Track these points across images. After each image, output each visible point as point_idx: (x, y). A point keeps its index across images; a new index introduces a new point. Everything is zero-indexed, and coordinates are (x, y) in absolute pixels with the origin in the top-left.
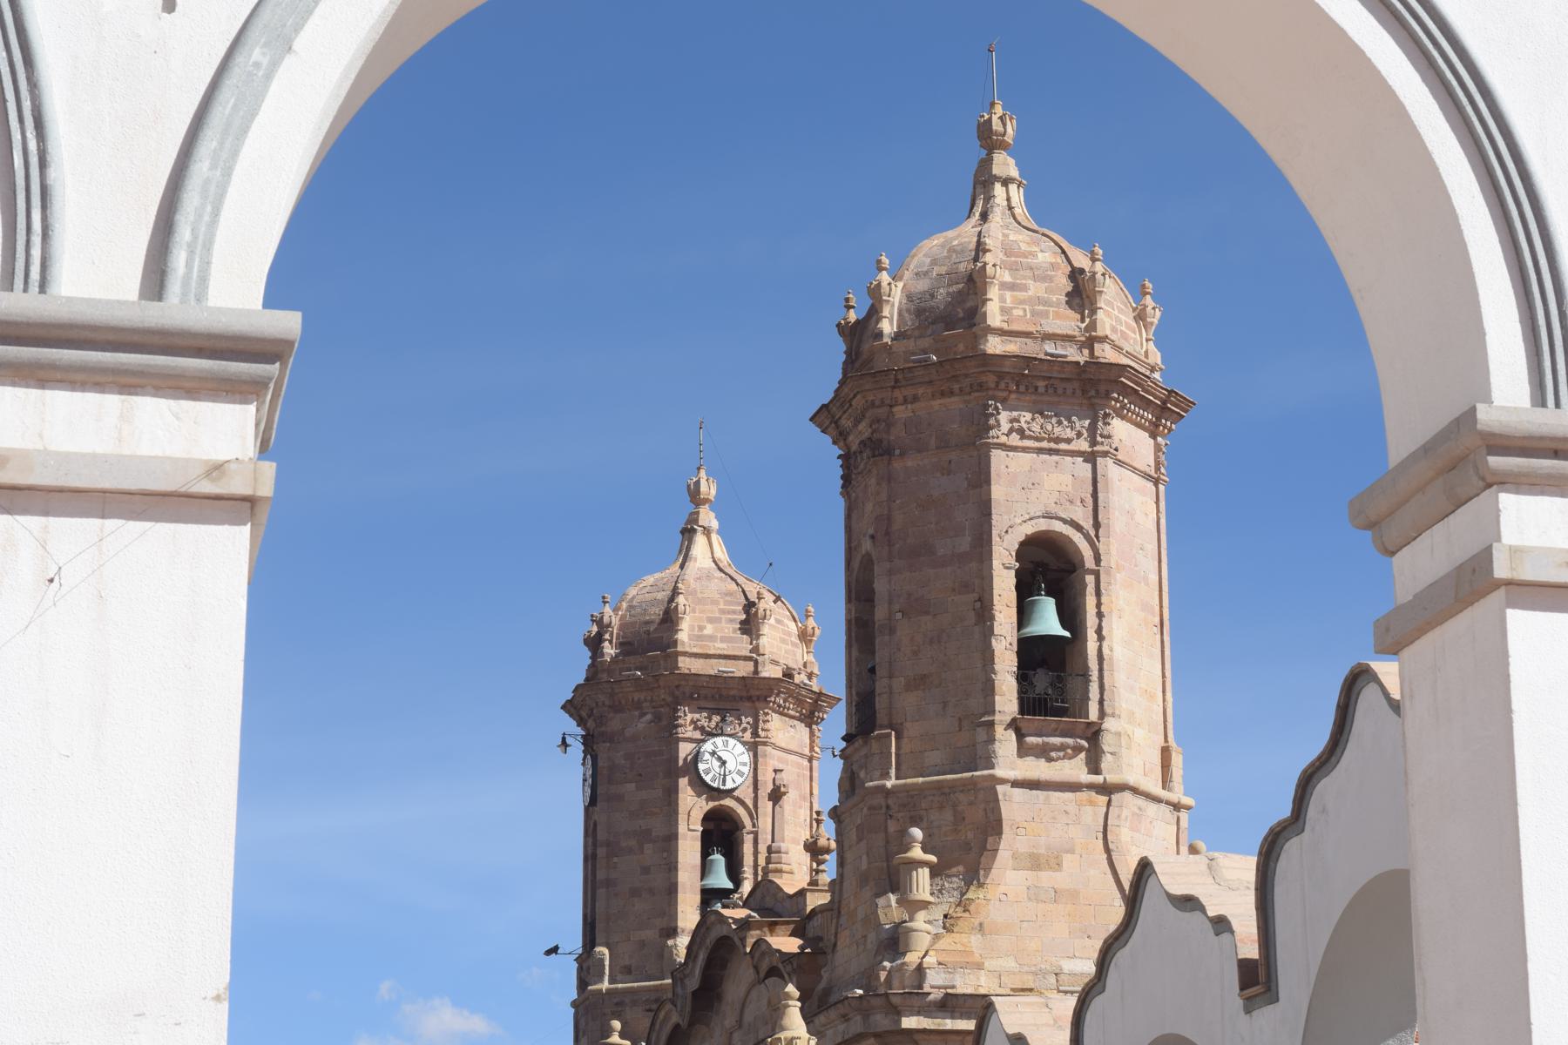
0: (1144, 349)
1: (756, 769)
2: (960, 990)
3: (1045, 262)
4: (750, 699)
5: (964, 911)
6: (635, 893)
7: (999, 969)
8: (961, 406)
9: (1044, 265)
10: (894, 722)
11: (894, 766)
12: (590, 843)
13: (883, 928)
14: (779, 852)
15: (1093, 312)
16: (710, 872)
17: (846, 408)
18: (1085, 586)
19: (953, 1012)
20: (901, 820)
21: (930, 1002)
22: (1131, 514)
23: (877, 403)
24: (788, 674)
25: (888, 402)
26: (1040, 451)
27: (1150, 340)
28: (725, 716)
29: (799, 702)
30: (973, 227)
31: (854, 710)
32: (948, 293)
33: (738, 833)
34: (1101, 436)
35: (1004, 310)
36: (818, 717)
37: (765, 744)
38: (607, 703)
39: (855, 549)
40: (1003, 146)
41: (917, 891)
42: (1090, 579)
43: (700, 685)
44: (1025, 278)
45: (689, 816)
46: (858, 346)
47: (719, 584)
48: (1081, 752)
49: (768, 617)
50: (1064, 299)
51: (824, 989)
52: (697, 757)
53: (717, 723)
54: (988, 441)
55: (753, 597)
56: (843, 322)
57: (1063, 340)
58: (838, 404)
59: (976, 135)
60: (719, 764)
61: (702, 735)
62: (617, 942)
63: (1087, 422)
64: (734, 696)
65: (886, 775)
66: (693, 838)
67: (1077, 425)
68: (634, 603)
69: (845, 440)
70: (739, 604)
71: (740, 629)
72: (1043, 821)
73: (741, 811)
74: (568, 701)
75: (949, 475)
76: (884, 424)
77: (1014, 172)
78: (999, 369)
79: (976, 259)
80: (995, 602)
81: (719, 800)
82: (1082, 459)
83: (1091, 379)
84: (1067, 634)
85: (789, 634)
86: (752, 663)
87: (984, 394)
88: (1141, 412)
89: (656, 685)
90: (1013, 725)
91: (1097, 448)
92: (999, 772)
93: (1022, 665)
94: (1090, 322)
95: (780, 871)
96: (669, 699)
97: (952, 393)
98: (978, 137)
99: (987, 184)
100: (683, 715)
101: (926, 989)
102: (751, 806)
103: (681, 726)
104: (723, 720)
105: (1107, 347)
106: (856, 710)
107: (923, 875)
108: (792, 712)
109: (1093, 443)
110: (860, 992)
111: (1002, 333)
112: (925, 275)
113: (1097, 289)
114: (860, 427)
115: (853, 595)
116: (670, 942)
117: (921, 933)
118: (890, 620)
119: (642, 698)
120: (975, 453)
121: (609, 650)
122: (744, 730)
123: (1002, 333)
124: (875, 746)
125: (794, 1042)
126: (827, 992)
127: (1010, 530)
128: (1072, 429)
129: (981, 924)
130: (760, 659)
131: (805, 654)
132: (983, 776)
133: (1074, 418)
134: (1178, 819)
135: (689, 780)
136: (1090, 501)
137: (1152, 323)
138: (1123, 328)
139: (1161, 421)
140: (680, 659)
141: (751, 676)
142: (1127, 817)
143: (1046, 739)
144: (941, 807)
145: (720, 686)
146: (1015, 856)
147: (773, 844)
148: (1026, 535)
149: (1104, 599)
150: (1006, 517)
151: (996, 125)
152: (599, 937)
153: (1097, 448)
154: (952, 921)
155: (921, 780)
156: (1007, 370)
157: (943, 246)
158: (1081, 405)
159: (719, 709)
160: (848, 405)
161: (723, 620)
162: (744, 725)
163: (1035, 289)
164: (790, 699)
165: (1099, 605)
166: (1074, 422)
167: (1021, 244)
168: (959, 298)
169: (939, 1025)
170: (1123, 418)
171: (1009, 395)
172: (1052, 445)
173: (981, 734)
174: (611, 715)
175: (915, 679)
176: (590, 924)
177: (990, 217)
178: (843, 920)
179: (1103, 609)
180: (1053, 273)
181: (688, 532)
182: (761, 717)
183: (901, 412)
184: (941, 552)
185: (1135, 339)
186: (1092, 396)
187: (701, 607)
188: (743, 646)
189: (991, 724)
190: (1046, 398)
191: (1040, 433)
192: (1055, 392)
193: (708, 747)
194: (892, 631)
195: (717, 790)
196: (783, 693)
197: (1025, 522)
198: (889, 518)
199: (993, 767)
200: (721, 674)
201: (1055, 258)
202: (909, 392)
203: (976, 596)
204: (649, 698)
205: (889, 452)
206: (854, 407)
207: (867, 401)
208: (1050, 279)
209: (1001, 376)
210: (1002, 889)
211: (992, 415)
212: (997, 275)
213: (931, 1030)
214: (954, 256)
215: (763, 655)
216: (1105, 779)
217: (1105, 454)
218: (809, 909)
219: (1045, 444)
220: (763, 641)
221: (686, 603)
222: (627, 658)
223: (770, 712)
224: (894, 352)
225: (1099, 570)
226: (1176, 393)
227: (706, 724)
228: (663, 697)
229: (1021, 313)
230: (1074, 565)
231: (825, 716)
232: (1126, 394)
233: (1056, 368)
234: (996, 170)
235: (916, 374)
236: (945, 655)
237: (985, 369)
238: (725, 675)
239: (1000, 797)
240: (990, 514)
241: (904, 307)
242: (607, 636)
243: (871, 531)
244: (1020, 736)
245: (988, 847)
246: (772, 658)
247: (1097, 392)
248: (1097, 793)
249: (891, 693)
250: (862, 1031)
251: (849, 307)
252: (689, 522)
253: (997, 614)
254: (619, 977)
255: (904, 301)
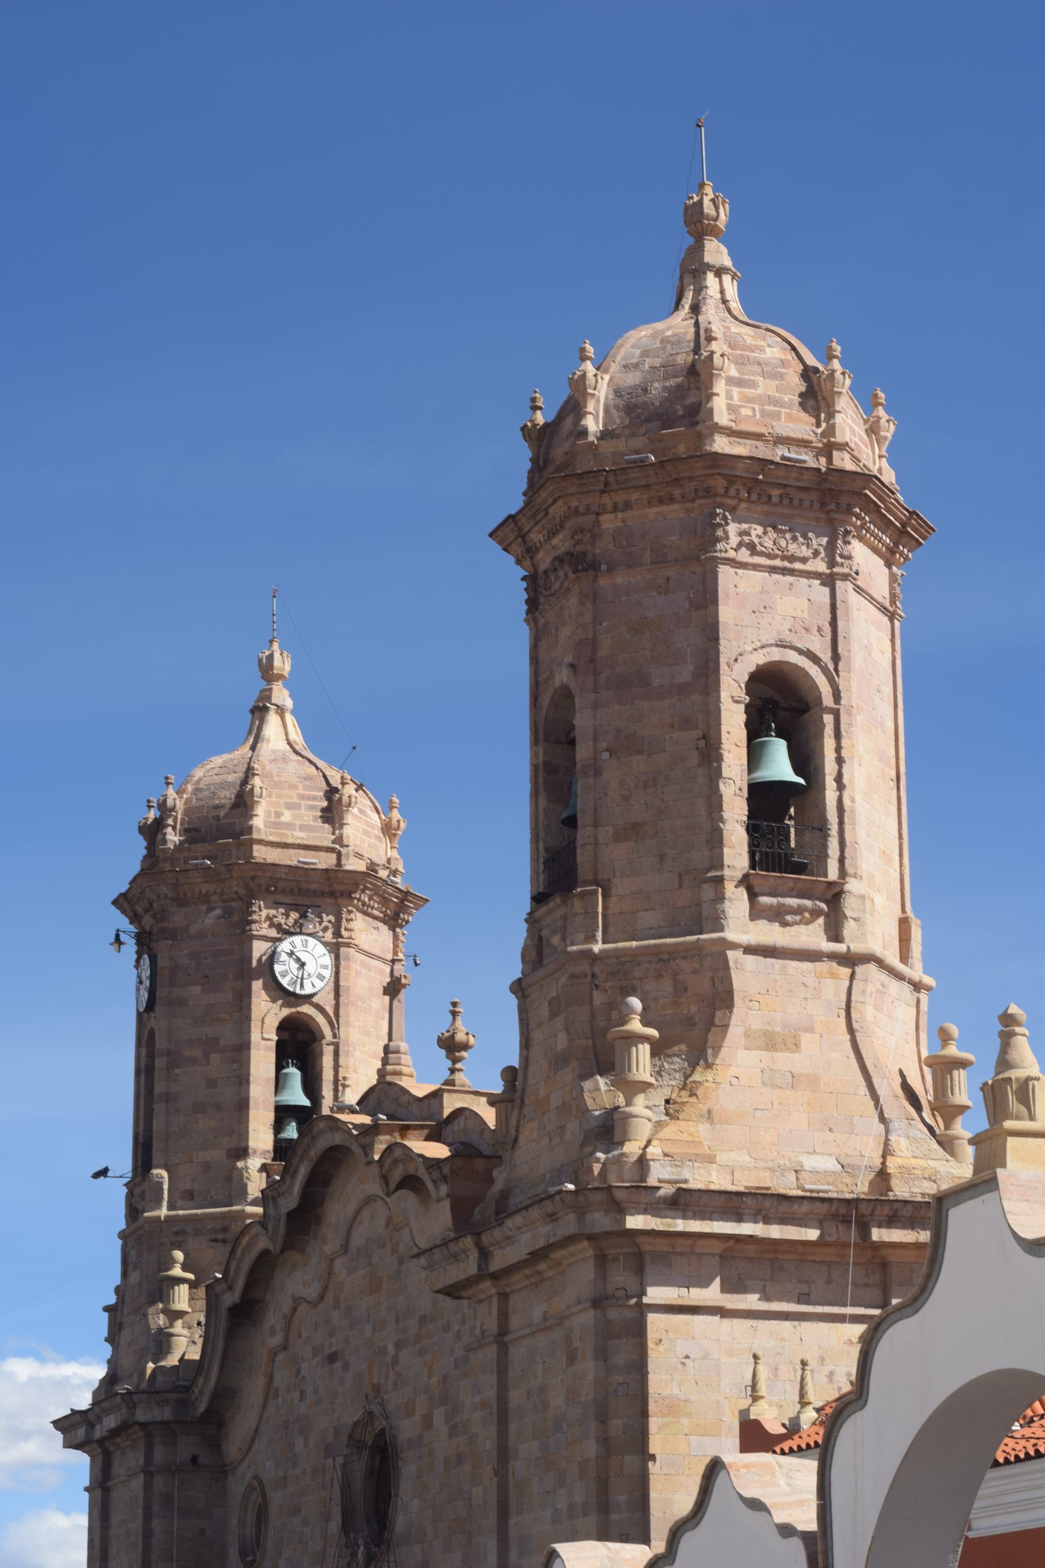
0: (877, 467)
1: (337, 974)
2: (693, 1185)
3: (775, 359)
4: (332, 894)
5: (691, 1095)
6: (199, 1108)
7: (731, 1164)
8: (682, 515)
9: (773, 361)
10: (600, 878)
11: (600, 929)
12: (144, 1054)
13: (592, 1115)
14: (398, 1052)
15: (831, 415)
16: (283, 1088)
17: (539, 518)
18: (822, 726)
19: (684, 1211)
20: (609, 991)
21: (660, 1198)
22: (868, 649)
23: (582, 510)
24: (372, 867)
25: (595, 508)
26: (773, 570)
27: (883, 456)
28: (306, 912)
29: (385, 901)
30: (683, 320)
31: (541, 867)
32: (664, 388)
33: (315, 1045)
34: (841, 556)
35: (731, 408)
36: (403, 920)
37: (348, 945)
38: (170, 895)
39: (546, 682)
40: (714, 232)
41: (637, 1071)
42: (828, 719)
43: (278, 876)
44: (753, 373)
45: (263, 1022)
46: (547, 453)
47: (296, 768)
48: (819, 916)
49: (353, 804)
50: (797, 399)
51: (501, 1192)
52: (272, 958)
53: (296, 922)
54: (715, 554)
55: (336, 782)
56: (529, 424)
57: (797, 446)
58: (530, 514)
59: (682, 219)
60: (298, 966)
61: (278, 933)
62: (178, 1164)
63: (824, 540)
64: (315, 891)
65: (592, 938)
66: (267, 1049)
67: (814, 542)
68: (201, 785)
69: (532, 558)
70: (319, 789)
71: (321, 817)
72: (779, 994)
73: (320, 1019)
74: (122, 895)
75: (666, 594)
76: (589, 534)
77: (728, 262)
78: (731, 472)
79: (696, 350)
80: (724, 740)
81: (296, 1007)
82: (819, 582)
83: (833, 490)
84: (801, 781)
85: (372, 826)
86: (334, 855)
87: (711, 501)
88: (880, 534)
89: (228, 876)
90: (745, 882)
91: (836, 570)
92: (731, 934)
93: (753, 813)
94: (826, 427)
95: (399, 1074)
96: (242, 892)
97: (671, 500)
98: (685, 222)
99: (697, 274)
100: (257, 910)
101: (652, 1181)
102: (332, 1015)
103: (255, 922)
104: (304, 916)
105: (847, 456)
106: (545, 868)
107: (644, 1051)
108: (376, 913)
109: (832, 563)
110: (571, 1187)
111: (731, 433)
112: (635, 367)
113: (836, 389)
114: (555, 541)
115: (541, 736)
116: (240, 1164)
117: (642, 1120)
118: (595, 759)
119: (211, 890)
120: (699, 569)
121: (173, 837)
122: (325, 929)
123: (731, 433)
124: (578, 905)
125: (1031, 1084)
126: (505, 1195)
127: (740, 658)
128: (808, 547)
129: (709, 1112)
130: (343, 851)
131: (389, 850)
132: (711, 940)
133: (810, 535)
134: (918, 1001)
135: (264, 984)
136: (827, 630)
137: (885, 438)
138: (857, 440)
139: (899, 548)
140: (256, 847)
141: (334, 868)
142: (871, 993)
143: (781, 900)
144: (659, 976)
145: (299, 879)
146: (747, 1034)
147: (391, 1043)
148: (758, 665)
149: (844, 742)
150: (734, 643)
151: (708, 208)
152: (157, 1156)
153: (836, 570)
154: (677, 1107)
155: (634, 944)
156: (738, 473)
157: (654, 336)
158: (818, 520)
159: (296, 905)
160: (542, 514)
161: (303, 807)
162: (325, 924)
163: (765, 387)
164: (375, 898)
165: (838, 749)
166: (811, 539)
167: (745, 337)
168: (678, 393)
169: (669, 1226)
170: (861, 539)
171: (738, 505)
172: (786, 564)
173: (708, 892)
174: (174, 909)
175: (625, 829)
176: (143, 1144)
177: (704, 309)
178: (527, 1111)
179: (844, 753)
180: (784, 370)
181: (259, 711)
182: (344, 916)
183: (609, 522)
184: (657, 682)
185: (868, 455)
186: (832, 510)
187: (278, 791)
188: (324, 836)
189: (720, 880)
190: (780, 510)
191: (772, 550)
192: (791, 503)
193: (285, 946)
194: (598, 773)
195: (293, 995)
196: (370, 890)
197: (755, 650)
198: (594, 643)
199: (722, 930)
200: (301, 865)
201: (785, 354)
202: (620, 498)
203: (699, 733)
204: (219, 890)
205: (594, 567)
206: (550, 516)
207: (569, 508)
208: (782, 377)
209: (731, 480)
210: (733, 1071)
211: (720, 525)
212: (725, 367)
213: (660, 1231)
214: (669, 347)
215: (347, 846)
216: (849, 948)
217: (845, 577)
218: (446, 1112)
219: (777, 563)
220: (347, 831)
221: (262, 785)
222: (193, 847)
223: (354, 910)
224: (600, 454)
225: (839, 709)
226: (918, 515)
227: (283, 921)
228: (235, 889)
229: (749, 413)
230: (807, 704)
231: (410, 919)
232: (869, 511)
233: (794, 475)
234: (708, 258)
235: (631, 476)
236: (663, 801)
237: (715, 471)
238: (306, 866)
239: (731, 964)
240: (717, 639)
241: (611, 402)
242: (170, 821)
243: (569, 659)
244: (752, 895)
245: (717, 1022)
246: (356, 850)
247: (838, 505)
248: (839, 964)
249: (596, 844)
250: (578, 1232)
251: (535, 408)
252: (259, 699)
253: (725, 754)
254: (179, 1202)
255: (611, 396)
